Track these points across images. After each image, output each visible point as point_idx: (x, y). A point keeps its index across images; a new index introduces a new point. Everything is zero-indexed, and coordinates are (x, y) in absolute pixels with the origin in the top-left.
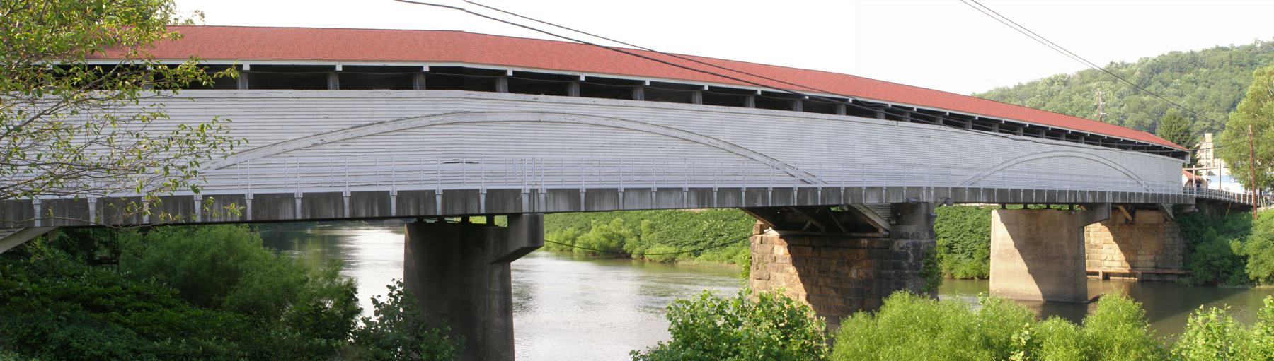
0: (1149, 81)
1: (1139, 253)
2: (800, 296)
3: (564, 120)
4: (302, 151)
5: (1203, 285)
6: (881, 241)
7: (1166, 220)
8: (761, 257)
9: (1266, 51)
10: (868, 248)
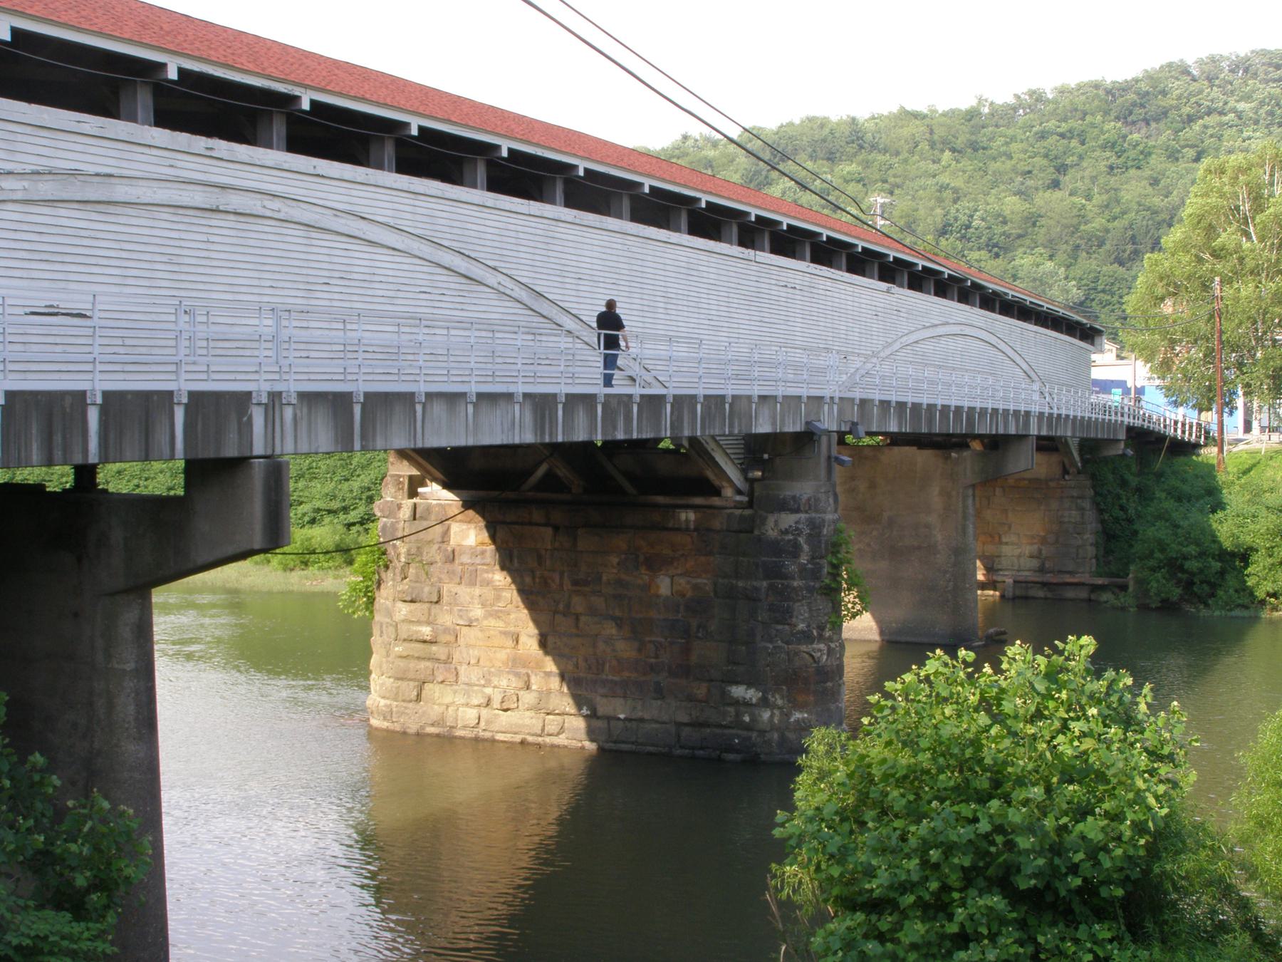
0: (766, 177)
1: (1004, 540)
2: (523, 639)
3: (261, 212)
5: (1157, 609)
6: (729, 516)
8: (413, 551)
9: (1001, 122)
10: (696, 529)
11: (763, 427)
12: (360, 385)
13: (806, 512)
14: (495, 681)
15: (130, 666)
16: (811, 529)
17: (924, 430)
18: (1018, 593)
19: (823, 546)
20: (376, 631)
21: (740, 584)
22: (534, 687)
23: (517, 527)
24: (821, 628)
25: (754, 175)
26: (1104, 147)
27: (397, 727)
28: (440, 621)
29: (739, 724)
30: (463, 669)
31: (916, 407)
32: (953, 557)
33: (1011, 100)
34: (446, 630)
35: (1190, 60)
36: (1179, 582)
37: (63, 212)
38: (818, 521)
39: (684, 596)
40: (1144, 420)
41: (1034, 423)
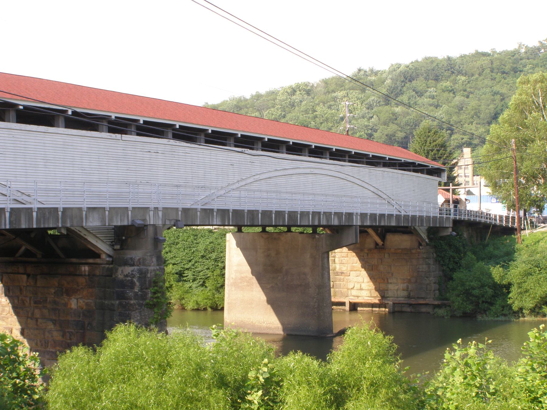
0: (401, 90)
1: (390, 281)
2: (14, 331)
5: (460, 317)
7: (420, 244)
9: (530, 57)
10: (89, 275)
13: (138, 266)
16: (140, 274)
19: (147, 283)
21: (106, 302)
23: (12, 275)
25: (394, 89)
32: (317, 290)
33: (537, 44)
38: (144, 270)
39: (82, 308)
40: (487, 218)
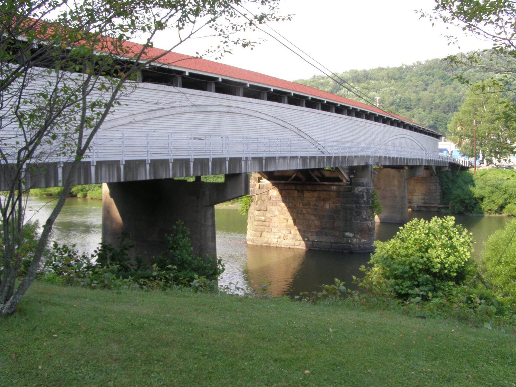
3: (238, 112)
4: (123, 127)
7: (431, 175)
11: (355, 164)
12: (265, 155)
14: (282, 231)
15: (210, 224)
17: (395, 164)
18: (418, 209)
20: (249, 218)
22: (292, 233)
24: (369, 217)
26: (440, 78)
27: (255, 244)
28: (267, 216)
29: (348, 243)
30: (273, 229)
31: (393, 158)
33: (412, 64)
34: (268, 218)
35: (465, 53)
36: (463, 206)
37: (197, 114)
41: (424, 162)
